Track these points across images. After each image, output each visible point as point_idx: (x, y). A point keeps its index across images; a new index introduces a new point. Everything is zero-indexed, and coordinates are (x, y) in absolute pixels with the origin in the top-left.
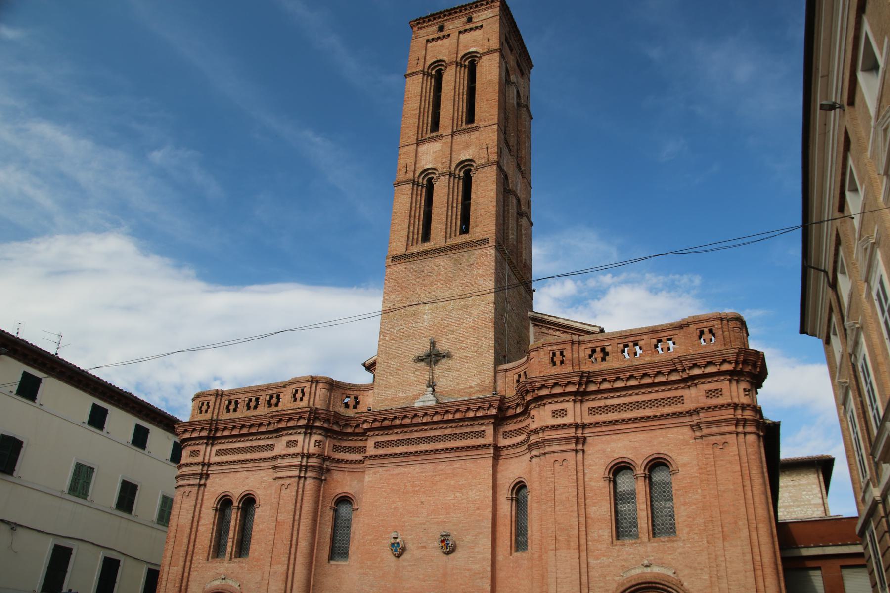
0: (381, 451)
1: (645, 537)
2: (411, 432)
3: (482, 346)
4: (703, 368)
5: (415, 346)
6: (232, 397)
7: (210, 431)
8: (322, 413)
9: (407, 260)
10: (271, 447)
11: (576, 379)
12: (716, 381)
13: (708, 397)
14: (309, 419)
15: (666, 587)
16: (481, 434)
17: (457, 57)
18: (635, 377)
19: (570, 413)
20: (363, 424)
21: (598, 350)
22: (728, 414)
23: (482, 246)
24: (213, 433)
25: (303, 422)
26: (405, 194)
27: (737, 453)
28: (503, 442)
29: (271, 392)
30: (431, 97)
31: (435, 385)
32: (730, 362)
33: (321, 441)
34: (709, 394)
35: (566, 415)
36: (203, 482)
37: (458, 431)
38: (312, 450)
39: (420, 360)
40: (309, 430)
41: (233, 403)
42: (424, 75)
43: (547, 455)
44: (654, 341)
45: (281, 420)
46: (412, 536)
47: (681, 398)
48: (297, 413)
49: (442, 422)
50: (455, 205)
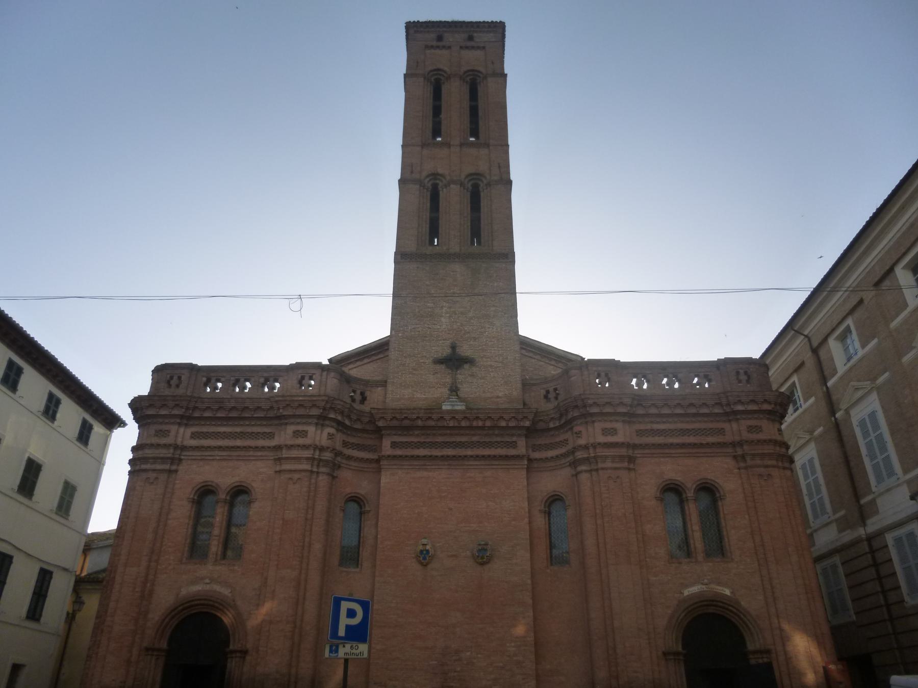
0: (399, 452)
1: (700, 557)
2: (434, 435)
5: (433, 348)
8: (339, 404)
12: (756, 418)
15: (726, 606)
16: (514, 445)
20: (379, 421)
22: (769, 449)
25: (315, 412)
31: (459, 390)
32: (770, 403)
33: (333, 435)
34: (750, 429)
36: (174, 468)
37: (487, 440)
38: (325, 442)
39: (439, 361)
40: (322, 420)
46: (441, 544)
47: (723, 431)
49: (471, 428)
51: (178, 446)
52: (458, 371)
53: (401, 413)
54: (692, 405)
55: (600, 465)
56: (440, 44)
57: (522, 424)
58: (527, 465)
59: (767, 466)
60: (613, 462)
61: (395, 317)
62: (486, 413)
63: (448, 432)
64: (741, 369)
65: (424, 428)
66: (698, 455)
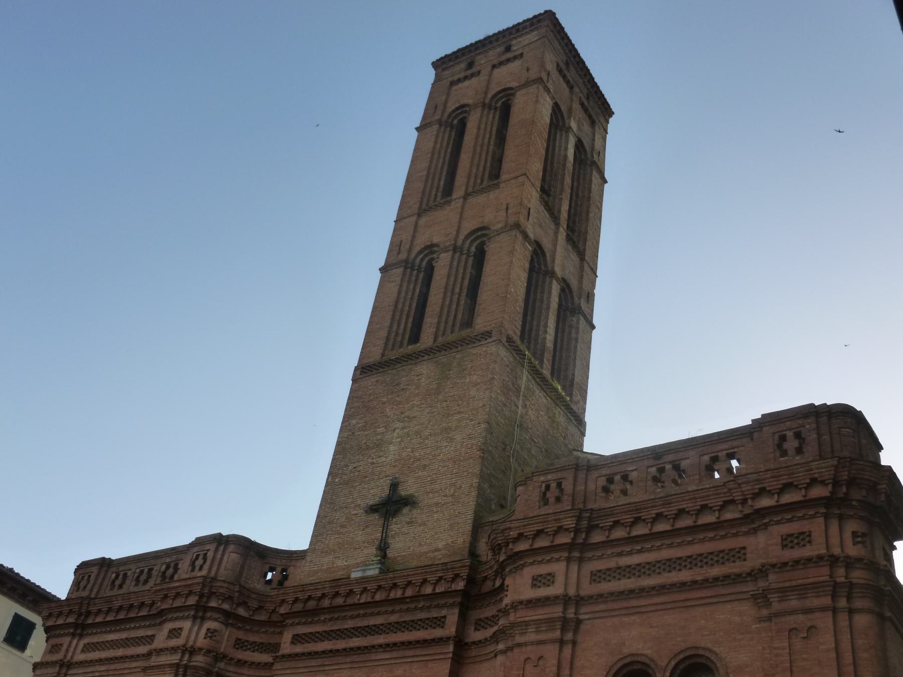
0: (299, 649)
3: (461, 487)
4: (776, 496)
5: (371, 491)
6: (121, 568)
7: (80, 615)
8: (221, 587)
9: (381, 370)
10: (152, 638)
11: (570, 523)
13: (786, 546)
14: (201, 596)
16: (439, 622)
17: (485, 98)
18: (666, 516)
19: (560, 580)
21: (617, 478)
22: (821, 574)
23: (482, 343)
24: (82, 618)
25: (192, 601)
26: (393, 282)
27: (833, 645)
28: (475, 635)
29: (168, 560)
30: (448, 155)
32: (823, 483)
33: (215, 631)
35: (553, 582)
37: (408, 618)
38: (201, 642)
39: (372, 509)
40: (200, 612)
41: (121, 577)
42: (441, 125)
43: (516, 650)
44: (706, 458)
45: (166, 596)
47: (743, 551)
48: (186, 586)
49: (387, 602)
50: (457, 290)
51: (570, 598)
52: (394, 520)
53: (303, 591)
54: (681, 512)
55: (519, 639)
56: (509, 55)
57: (454, 587)
58: (453, 653)
59: (808, 611)
60: (538, 632)
61: (337, 456)
62: (404, 576)
63: (362, 612)
64: (790, 429)
65: (332, 609)
66: (689, 604)
